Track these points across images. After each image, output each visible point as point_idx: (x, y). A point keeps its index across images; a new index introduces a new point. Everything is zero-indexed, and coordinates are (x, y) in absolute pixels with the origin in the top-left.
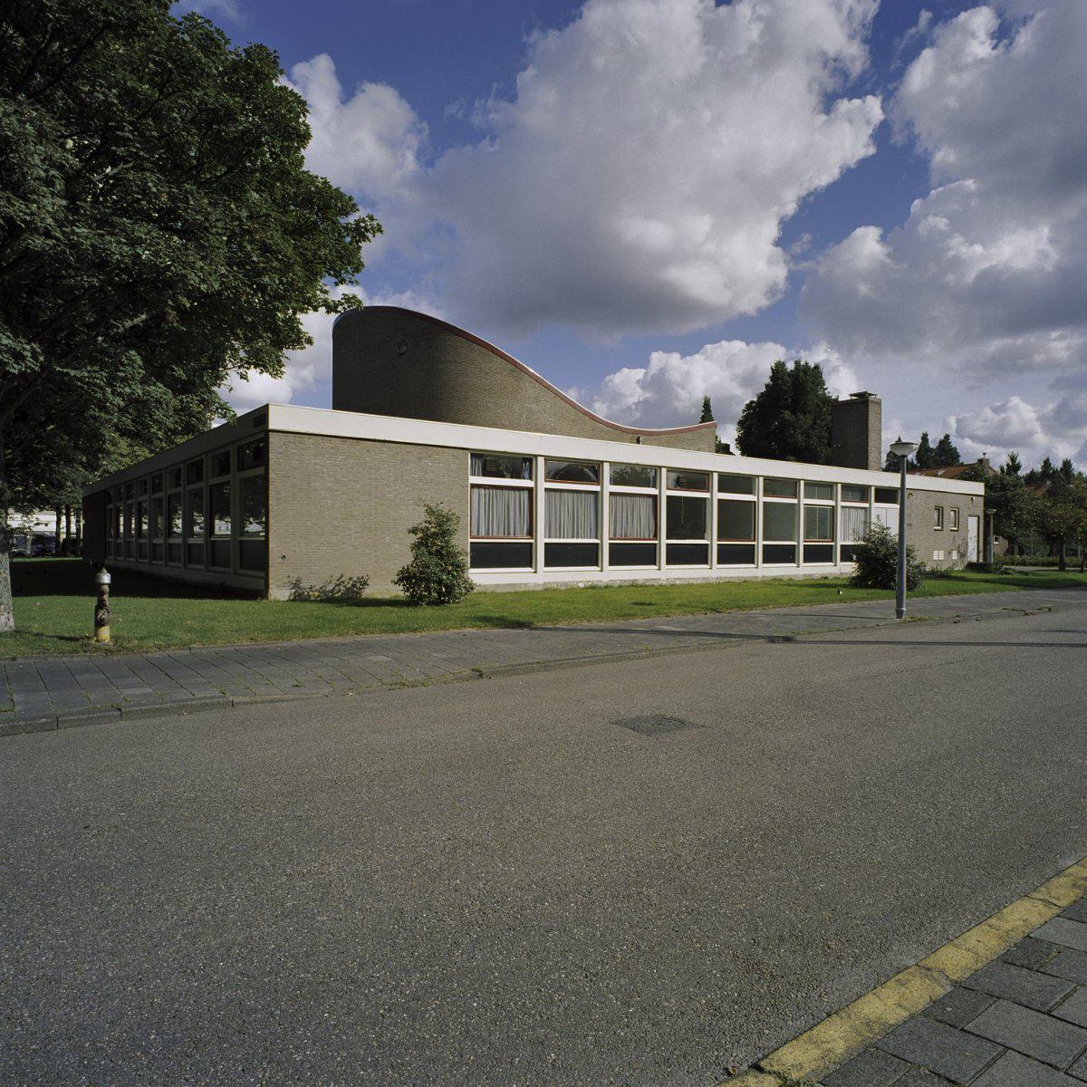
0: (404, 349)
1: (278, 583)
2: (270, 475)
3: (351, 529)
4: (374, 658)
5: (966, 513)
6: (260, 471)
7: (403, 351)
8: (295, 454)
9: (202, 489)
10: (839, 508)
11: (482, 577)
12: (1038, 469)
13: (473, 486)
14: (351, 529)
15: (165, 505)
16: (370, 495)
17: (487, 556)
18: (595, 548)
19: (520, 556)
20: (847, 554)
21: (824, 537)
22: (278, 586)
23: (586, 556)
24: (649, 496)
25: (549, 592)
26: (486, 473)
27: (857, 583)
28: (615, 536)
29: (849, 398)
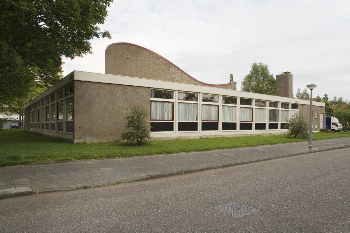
0: (129, 57)
1: (78, 137)
2: (75, 97)
3: (106, 117)
4: (105, 169)
5: (320, 113)
6: (71, 96)
7: (128, 57)
8: (84, 89)
9: (55, 103)
10: (291, 111)
11: (155, 135)
12: (332, 100)
13: (151, 101)
14: (106, 117)
15: (56, 108)
16: (112, 104)
17: (159, 126)
18: (196, 124)
19: (168, 127)
20: (283, 126)
21: (275, 121)
22: (78, 138)
23: (192, 127)
24: (171, 102)
25: (177, 140)
26: (156, 97)
27: (288, 137)
28: (218, 96)
29: (282, 74)
